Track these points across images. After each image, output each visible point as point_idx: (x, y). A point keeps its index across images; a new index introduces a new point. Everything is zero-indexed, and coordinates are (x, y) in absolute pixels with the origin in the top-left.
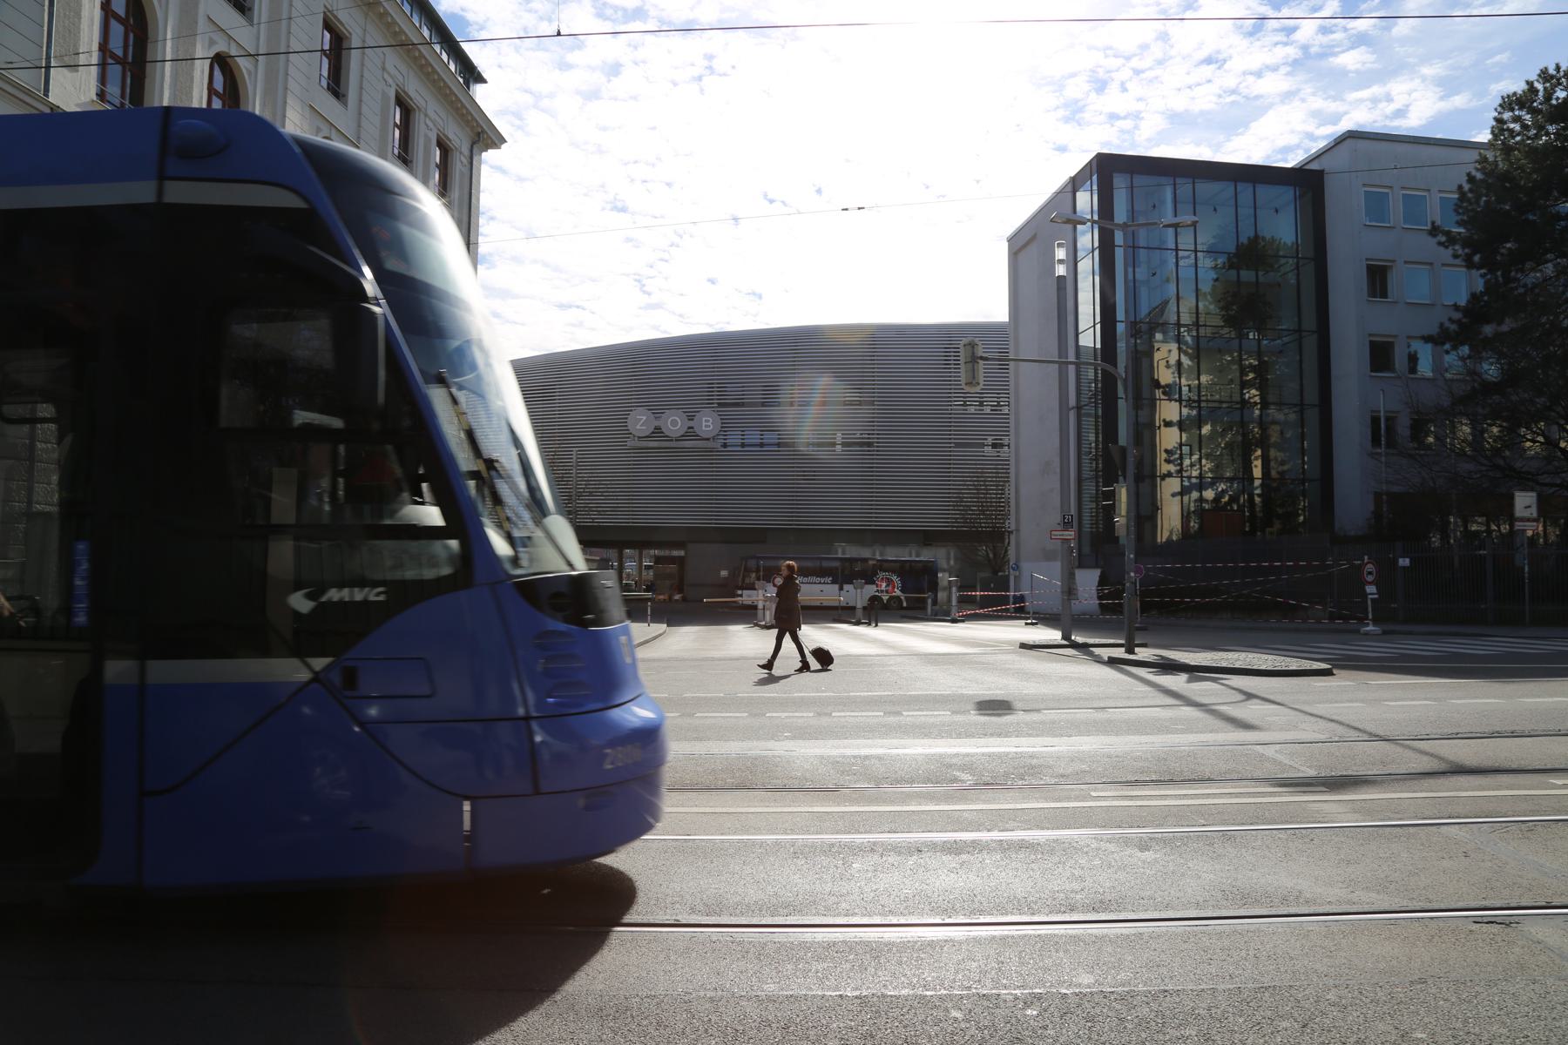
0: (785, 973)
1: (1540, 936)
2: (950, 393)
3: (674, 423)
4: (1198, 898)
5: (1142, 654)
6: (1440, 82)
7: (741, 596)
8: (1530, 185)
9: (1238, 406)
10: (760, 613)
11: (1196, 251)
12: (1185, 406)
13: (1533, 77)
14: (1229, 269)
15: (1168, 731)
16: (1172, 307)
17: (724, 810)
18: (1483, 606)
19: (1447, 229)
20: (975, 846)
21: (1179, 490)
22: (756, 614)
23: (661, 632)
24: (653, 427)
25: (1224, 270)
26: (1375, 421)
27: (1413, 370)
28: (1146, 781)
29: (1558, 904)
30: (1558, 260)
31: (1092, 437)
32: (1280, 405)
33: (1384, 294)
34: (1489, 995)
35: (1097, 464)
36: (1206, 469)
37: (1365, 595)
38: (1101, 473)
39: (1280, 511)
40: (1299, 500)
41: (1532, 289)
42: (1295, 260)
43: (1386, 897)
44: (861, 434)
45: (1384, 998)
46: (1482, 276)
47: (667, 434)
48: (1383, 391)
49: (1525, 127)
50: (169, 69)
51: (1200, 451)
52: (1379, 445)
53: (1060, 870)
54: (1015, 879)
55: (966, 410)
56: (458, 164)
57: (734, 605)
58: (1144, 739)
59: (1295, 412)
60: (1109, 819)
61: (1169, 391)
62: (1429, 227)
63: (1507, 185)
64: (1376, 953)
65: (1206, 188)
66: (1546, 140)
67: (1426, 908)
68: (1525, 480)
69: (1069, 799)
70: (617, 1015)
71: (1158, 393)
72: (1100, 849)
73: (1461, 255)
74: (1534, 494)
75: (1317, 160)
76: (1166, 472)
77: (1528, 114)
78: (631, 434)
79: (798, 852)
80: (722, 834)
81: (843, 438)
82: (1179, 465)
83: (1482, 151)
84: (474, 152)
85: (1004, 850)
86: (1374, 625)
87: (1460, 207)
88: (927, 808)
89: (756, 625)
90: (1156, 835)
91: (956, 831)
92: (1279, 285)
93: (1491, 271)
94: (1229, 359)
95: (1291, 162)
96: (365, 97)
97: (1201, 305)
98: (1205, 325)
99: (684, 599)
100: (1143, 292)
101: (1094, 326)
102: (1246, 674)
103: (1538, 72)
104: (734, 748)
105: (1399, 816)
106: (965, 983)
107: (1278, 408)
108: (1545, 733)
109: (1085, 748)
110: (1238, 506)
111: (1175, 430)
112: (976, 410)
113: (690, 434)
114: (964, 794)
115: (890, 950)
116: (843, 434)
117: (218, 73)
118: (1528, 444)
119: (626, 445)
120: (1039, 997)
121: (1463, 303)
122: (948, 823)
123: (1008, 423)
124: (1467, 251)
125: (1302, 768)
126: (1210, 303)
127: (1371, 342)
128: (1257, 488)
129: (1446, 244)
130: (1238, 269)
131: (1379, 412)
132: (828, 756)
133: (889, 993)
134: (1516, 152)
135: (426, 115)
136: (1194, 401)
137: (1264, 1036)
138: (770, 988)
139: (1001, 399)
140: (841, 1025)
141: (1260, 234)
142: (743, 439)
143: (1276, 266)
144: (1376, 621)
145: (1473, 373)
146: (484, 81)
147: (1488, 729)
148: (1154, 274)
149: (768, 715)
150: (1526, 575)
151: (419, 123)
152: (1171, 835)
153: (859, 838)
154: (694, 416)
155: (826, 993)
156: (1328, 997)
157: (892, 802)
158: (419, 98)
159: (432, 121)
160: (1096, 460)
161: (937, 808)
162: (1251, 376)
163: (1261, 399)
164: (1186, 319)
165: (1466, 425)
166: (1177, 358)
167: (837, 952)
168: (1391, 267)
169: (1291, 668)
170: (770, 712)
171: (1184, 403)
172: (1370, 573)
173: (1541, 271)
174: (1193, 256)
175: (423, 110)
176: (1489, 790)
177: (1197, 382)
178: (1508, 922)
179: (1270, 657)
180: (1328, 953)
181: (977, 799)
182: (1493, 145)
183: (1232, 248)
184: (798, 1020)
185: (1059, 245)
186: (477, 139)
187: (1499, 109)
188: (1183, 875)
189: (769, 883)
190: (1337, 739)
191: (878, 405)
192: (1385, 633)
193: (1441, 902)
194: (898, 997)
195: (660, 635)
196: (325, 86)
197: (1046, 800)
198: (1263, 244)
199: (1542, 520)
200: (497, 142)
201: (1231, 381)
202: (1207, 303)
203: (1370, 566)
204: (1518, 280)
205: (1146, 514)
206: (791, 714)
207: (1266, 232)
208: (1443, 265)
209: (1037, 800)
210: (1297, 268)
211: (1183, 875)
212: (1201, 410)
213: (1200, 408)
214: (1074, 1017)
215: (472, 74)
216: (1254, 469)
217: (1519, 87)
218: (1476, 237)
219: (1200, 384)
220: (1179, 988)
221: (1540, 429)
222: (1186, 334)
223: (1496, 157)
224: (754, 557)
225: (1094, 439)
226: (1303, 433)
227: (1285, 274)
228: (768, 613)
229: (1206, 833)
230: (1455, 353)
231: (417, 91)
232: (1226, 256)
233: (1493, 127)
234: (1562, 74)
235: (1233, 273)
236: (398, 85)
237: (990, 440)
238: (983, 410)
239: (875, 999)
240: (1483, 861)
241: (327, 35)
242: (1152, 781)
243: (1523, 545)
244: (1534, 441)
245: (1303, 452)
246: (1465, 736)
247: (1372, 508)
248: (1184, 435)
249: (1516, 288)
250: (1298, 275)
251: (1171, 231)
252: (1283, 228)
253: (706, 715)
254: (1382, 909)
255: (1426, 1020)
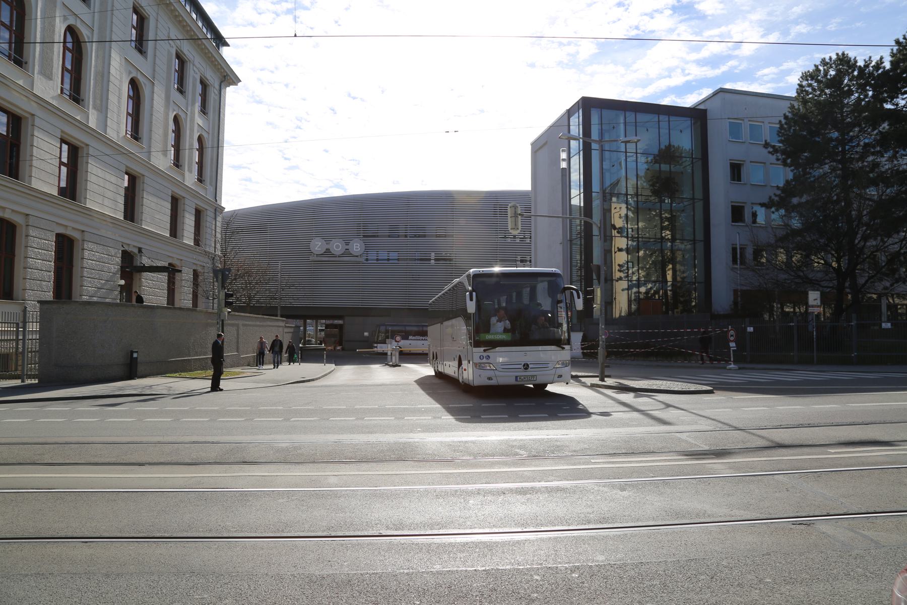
0: (444, 559)
1: (824, 530)
2: (497, 231)
3: (337, 247)
4: (654, 515)
5: (609, 381)
6: (760, 23)
7: (376, 347)
8: (817, 122)
9: (660, 240)
10: (389, 357)
11: (636, 153)
12: (630, 240)
13: (818, 63)
14: (654, 164)
15: (628, 425)
16: (623, 183)
17: (393, 473)
18: (792, 354)
19: (773, 144)
20: (533, 490)
21: (627, 287)
22: (387, 358)
23: (332, 369)
24: (325, 249)
25: (652, 164)
26: (734, 250)
27: (754, 222)
28: (620, 454)
29: (833, 514)
30: (832, 163)
31: (578, 257)
32: (683, 240)
33: (739, 179)
34: (800, 560)
35: (581, 272)
36: (641, 275)
37: (729, 348)
38: (583, 277)
39: (682, 299)
40: (692, 293)
41: (818, 179)
42: (691, 159)
43: (749, 513)
44: (446, 254)
45: (750, 563)
46: (792, 171)
47: (333, 253)
48: (739, 233)
49: (814, 90)
50: (39, 34)
51: (638, 265)
52: (737, 264)
53: (580, 501)
54: (557, 507)
55: (506, 240)
56: (213, 95)
57: (372, 352)
58: (616, 430)
59: (690, 244)
60: (602, 474)
61: (620, 231)
62: (764, 143)
63: (805, 121)
64: (745, 541)
65: (642, 117)
66: (825, 98)
67: (769, 518)
68: (815, 284)
69: (580, 464)
70: (359, 584)
71: (614, 233)
72: (599, 491)
73: (780, 159)
74: (819, 293)
75: (703, 104)
76: (619, 277)
77: (816, 82)
78: (312, 253)
79: (439, 495)
80: (395, 486)
81: (435, 256)
82: (626, 273)
83: (792, 102)
84: (222, 87)
85: (549, 492)
86: (734, 365)
87: (780, 132)
88: (504, 470)
89: (387, 364)
90: (628, 483)
91: (522, 482)
92: (682, 173)
93: (796, 168)
94: (654, 213)
95: (689, 101)
96: (158, 53)
97: (639, 183)
98: (641, 195)
99: (343, 349)
100: (607, 175)
101: (580, 195)
102: (667, 393)
103: (821, 60)
104: (391, 438)
105: (753, 470)
106: (539, 562)
107: (681, 242)
108: (825, 425)
109: (585, 435)
110: (659, 297)
111: (624, 254)
112: (511, 241)
113: (347, 253)
114: (522, 462)
115: (497, 546)
116: (435, 254)
117: (69, 39)
118: (816, 264)
119: (309, 259)
120: (578, 568)
121: (781, 185)
122: (517, 478)
123: (530, 248)
124: (783, 157)
125: (701, 445)
126: (644, 182)
127: (732, 206)
128: (669, 286)
129: (773, 153)
130: (660, 164)
131: (737, 245)
132: (445, 442)
133: (500, 568)
134: (809, 104)
135: (194, 65)
136: (636, 238)
137: (693, 583)
138: (438, 567)
139: (526, 235)
140: (478, 585)
141: (672, 144)
142: (377, 256)
143: (680, 162)
144: (735, 362)
145: (787, 225)
146: (229, 46)
147: (796, 423)
148: (613, 166)
149: (365, 419)
150: (815, 337)
151: (189, 69)
152: (636, 482)
153: (470, 487)
154: (349, 242)
155: (467, 569)
156: (723, 563)
157: (484, 467)
158: (189, 54)
159: (197, 69)
160: (581, 270)
161: (509, 470)
162: (666, 223)
163: (671, 236)
164: (631, 191)
165: (783, 253)
166: (626, 213)
167: (469, 548)
168: (743, 164)
169: (691, 390)
170: (406, 417)
171: (629, 239)
172: (732, 336)
173: (822, 168)
174: (635, 156)
175: (192, 61)
176: (812, 455)
177: (636, 226)
178: (808, 524)
179: (680, 383)
180: (722, 542)
181: (531, 464)
182: (797, 99)
183: (656, 152)
184: (455, 583)
185: (563, 151)
186: (224, 79)
187: (801, 79)
188: (644, 503)
189: (426, 513)
190: (718, 429)
191: (455, 237)
192: (740, 369)
193: (776, 514)
194: (505, 570)
195: (333, 371)
196: (134, 47)
197: (568, 464)
198: (673, 149)
199: (822, 306)
200: (235, 81)
201: (656, 226)
202: (642, 182)
203: (732, 331)
204: (810, 173)
205: (609, 302)
206: (419, 418)
207: (675, 142)
208: (771, 164)
209: (563, 465)
210: (692, 163)
211: (644, 503)
212: (638, 243)
213: (638, 241)
214: (597, 577)
215: (220, 41)
216: (668, 276)
217: (811, 69)
218: (788, 149)
219: (638, 227)
220: (648, 561)
221: (822, 256)
222: (630, 200)
223: (799, 106)
224: (384, 325)
225: (579, 258)
226: (695, 255)
227: (685, 167)
228: (394, 358)
229: (654, 481)
230: (777, 213)
231: (188, 49)
232: (653, 156)
233: (797, 89)
234: (833, 62)
235: (657, 166)
236: (177, 47)
237: (519, 258)
238: (515, 241)
239: (493, 571)
240: (796, 493)
241: (135, 17)
242: (623, 453)
243: (813, 319)
244: (818, 263)
245: (695, 266)
246: (785, 427)
247: (732, 298)
248: (629, 256)
249: (809, 178)
250: (693, 167)
251: (623, 145)
252: (684, 140)
253: (371, 418)
254: (747, 519)
255: (771, 573)
